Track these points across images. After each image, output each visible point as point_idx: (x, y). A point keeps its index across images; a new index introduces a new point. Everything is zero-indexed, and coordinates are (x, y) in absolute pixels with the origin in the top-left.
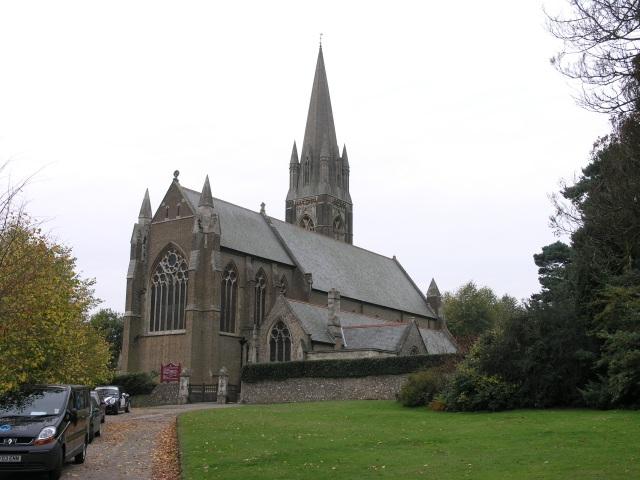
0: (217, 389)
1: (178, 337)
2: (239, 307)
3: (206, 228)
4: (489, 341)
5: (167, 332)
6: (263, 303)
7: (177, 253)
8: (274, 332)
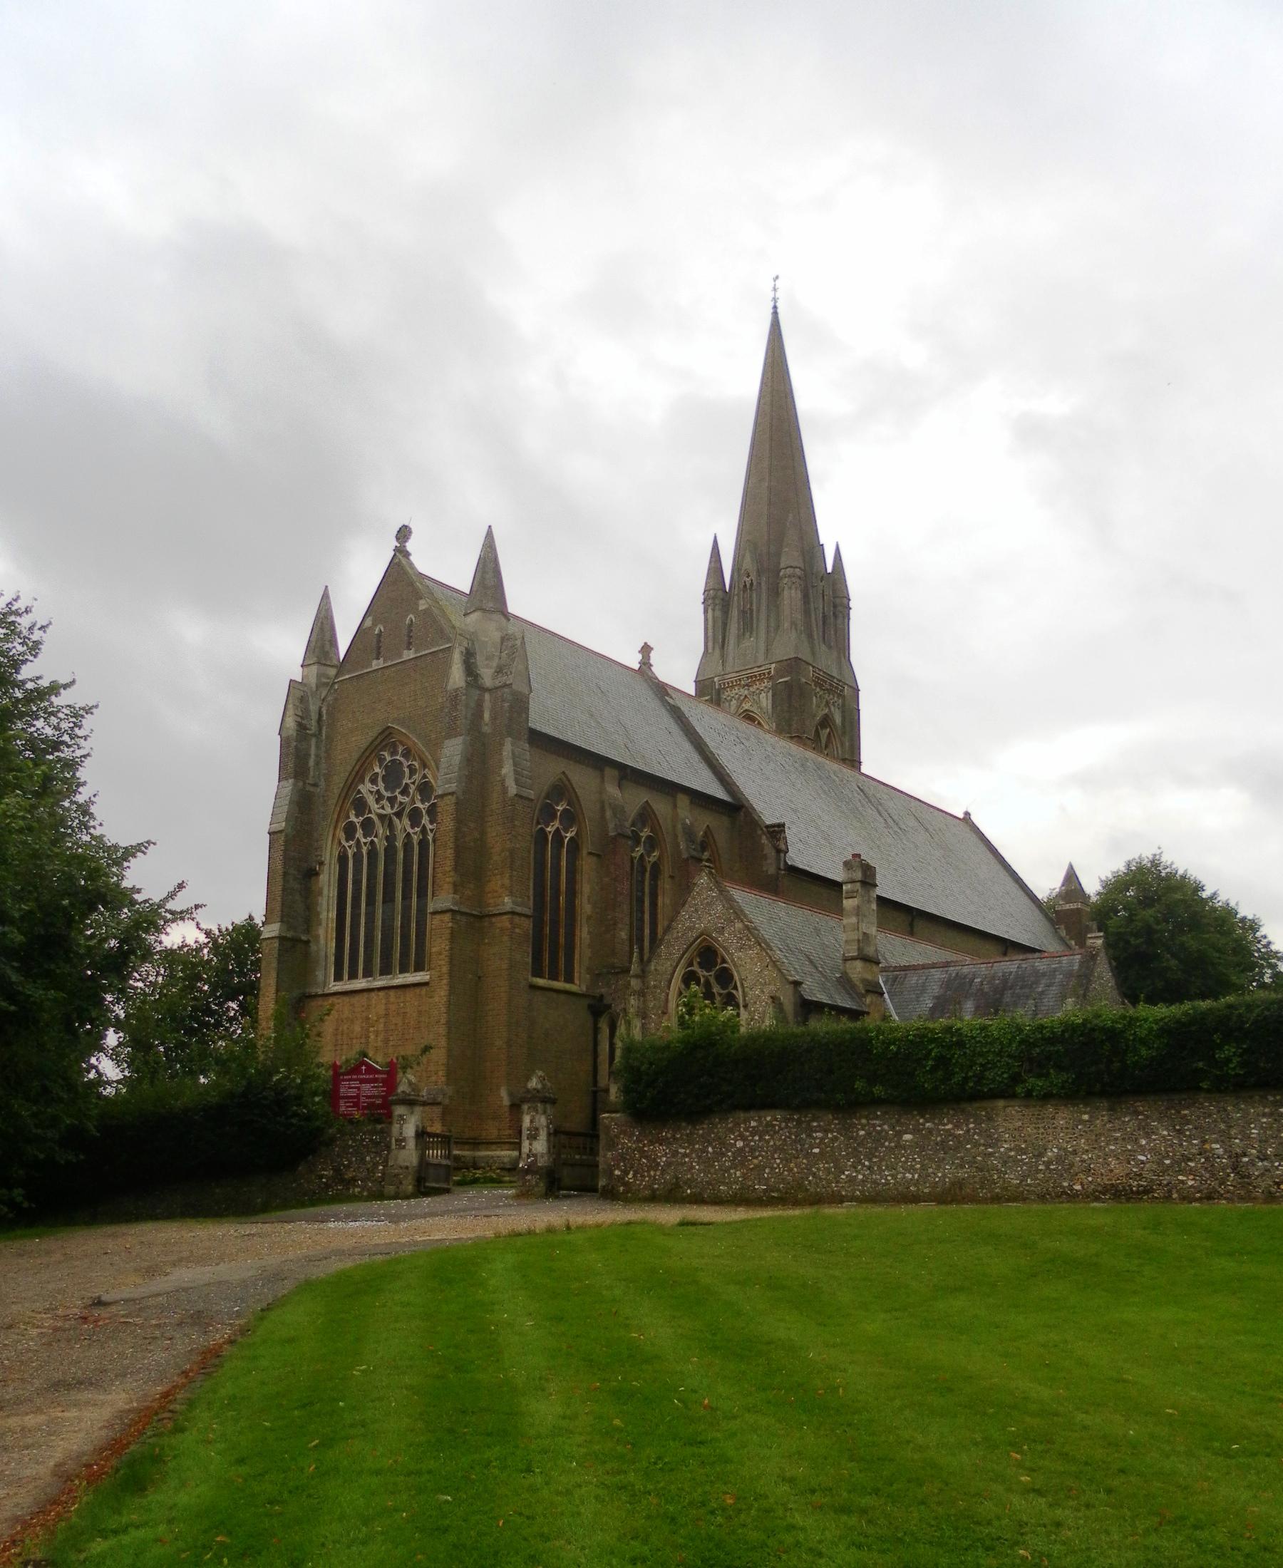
0: (518, 1146)
1: (410, 994)
3: (487, 676)
4: (589, 918)
5: (380, 982)
6: (654, 904)
7: (407, 754)
8: (689, 978)
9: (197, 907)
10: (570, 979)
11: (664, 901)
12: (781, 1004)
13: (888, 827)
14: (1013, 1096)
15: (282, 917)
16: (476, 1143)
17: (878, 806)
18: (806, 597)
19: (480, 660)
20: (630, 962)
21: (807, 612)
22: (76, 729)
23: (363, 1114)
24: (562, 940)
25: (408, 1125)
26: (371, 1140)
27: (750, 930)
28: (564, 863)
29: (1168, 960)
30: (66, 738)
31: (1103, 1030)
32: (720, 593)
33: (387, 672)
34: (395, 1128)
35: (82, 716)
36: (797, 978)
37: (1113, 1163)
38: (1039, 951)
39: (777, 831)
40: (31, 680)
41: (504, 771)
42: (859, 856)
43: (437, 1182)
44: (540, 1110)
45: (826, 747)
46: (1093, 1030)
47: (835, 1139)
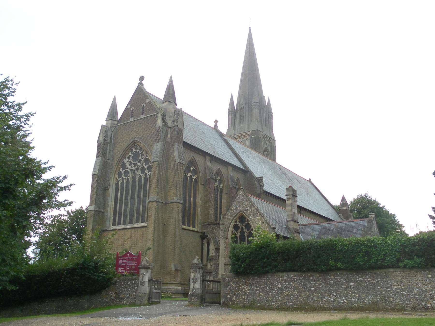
1: (139, 230)
2: (200, 202)
3: (169, 123)
4: (200, 206)
6: (221, 202)
7: (141, 149)
8: (236, 227)
9: (71, 185)
11: (224, 201)
13: (289, 181)
14: (398, 267)
18: (260, 112)
19: (167, 118)
21: (260, 116)
22: (27, 121)
23: (128, 272)
25: (146, 277)
26: (131, 282)
28: (193, 187)
30: (23, 124)
32: (233, 110)
33: (135, 122)
34: (141, 278)
35: (30, 117)
39: (260, 179)
40: (11, 102)
41: (175, 154)
42: (291, 186)
43: (156, 299)
47: (321, 284)
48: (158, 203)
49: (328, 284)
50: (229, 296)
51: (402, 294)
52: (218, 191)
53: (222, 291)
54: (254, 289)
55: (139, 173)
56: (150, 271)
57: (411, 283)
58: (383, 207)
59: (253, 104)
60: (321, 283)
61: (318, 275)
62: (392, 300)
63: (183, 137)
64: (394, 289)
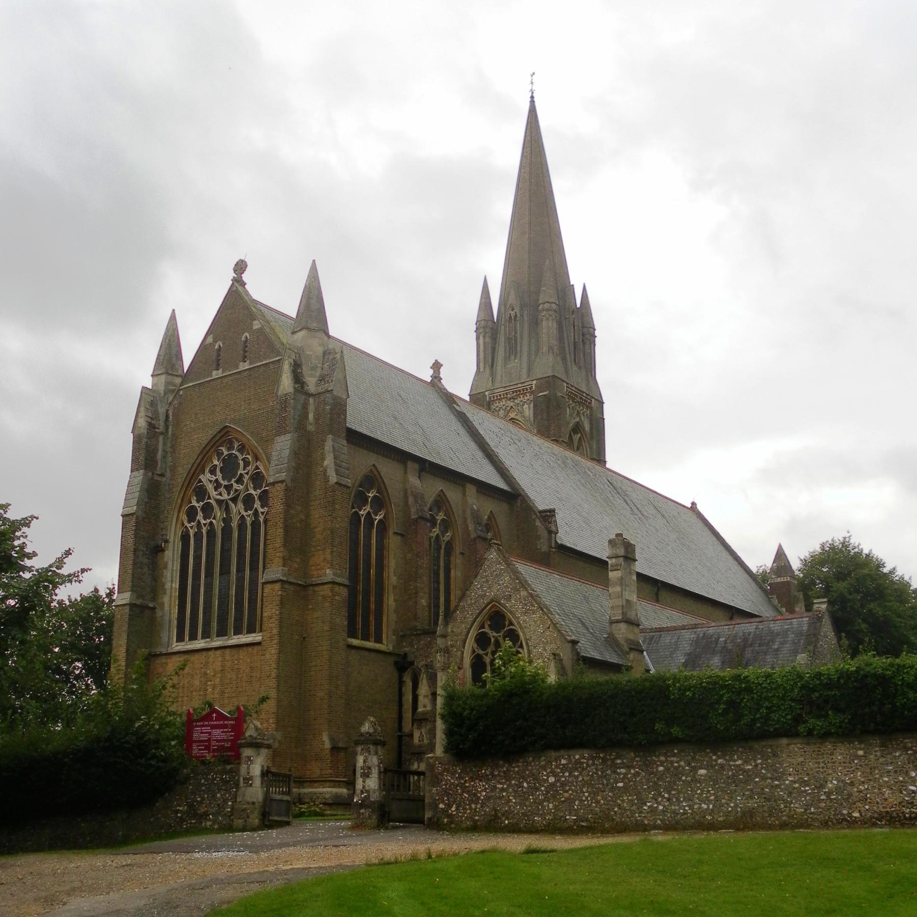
0: (351, 784)
1: (243, 653)
2: (394, 580)
3: (312, 384)
4: (395, 587)
5: (218, 642)
7: (242, 449)
8: (482, 640)
9: (83, 571)
10: (379, 640)
11: (456, 574)
12: (561, 660)
13: (633, 513)
14: (797, 735)
15: (133, 586)
16: (301, 782)
17: (624, 496)
19: (305, 370)
20: (436, 624)
21: (561, 339)
23: (214, 756)
24: (373, 606)
26: (222, 779)
27: (533, 597)
28: (374, 541)
29: (859, 624)
31: (875, 676)
32: (490, 323)
33: (225, 381)
34: (243, 767)
36: (573, 638)
37: (887, 792)
38: (756, 616)
39: (548, 516)
41: (326, 463)
42: (621, 535)
43: (280, 815)
44: (372, 752)
45: (578, 449)
46: (865, 676)
47: (637, 774)
48: (287, 586)
49: (652, 773)
50: (441, 806)
51: (803, 792)
52: (438, 549)
53: (427, 794)
54: (495, 787)
55: (237, 509)
56: (264, 751)
57: (823, 768)
58: (892, 571)
59: (540, 307)
60: (637, 772)
61: (632, 755)
62: (782, 806)
63: (345, 419)
64: (787, 782)
